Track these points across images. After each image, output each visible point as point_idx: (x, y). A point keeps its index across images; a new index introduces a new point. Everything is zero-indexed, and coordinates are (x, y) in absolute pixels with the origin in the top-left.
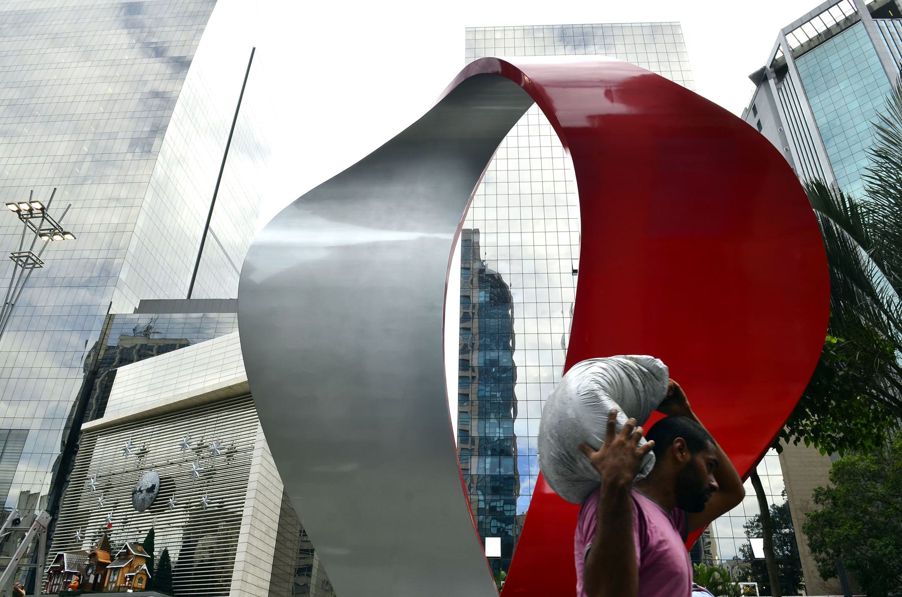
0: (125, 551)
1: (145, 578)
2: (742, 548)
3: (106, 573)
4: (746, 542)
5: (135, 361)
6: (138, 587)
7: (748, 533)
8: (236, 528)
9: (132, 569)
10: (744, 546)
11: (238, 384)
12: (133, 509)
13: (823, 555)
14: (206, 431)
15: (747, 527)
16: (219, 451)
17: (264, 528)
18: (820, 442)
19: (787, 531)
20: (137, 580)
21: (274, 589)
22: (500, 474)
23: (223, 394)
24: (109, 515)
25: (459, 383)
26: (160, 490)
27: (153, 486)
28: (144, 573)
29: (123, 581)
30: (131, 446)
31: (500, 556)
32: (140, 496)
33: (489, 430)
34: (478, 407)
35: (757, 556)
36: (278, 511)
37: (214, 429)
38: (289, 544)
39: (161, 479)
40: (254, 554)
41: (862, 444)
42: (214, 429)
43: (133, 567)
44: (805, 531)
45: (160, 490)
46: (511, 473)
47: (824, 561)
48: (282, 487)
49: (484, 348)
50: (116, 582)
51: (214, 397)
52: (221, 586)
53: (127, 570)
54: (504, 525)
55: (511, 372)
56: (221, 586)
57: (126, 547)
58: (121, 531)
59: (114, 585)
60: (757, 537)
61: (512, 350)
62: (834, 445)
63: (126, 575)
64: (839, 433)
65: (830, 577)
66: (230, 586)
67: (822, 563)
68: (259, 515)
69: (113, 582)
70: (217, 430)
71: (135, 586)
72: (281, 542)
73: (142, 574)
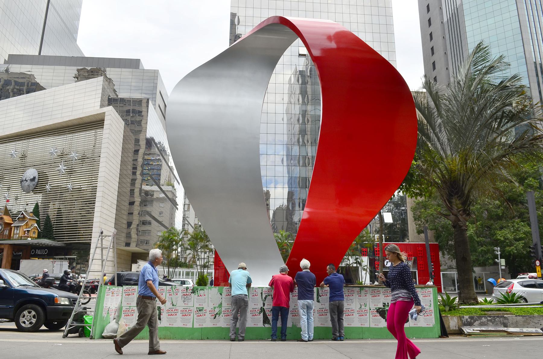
0: (22, 216)
1: (37, 231)
3: (11, 228)
5: (11, 97)
6: (33, 236)
9: (28, 227)
11: (86, 117)
12: (21, 191)
13: (420, 222)
16: (76, 158)
17: (109, 203)
19: (404, 208)
20: (32, 233)
23: (76, 122)
24: (6, 194)
26: (39, 180)
27: (34, 178)
28: (36, 228)
29: (23, 233)
30: (16, 153)
32: (27, 184)
38: (123, 212)
39: (39, 173)
40: (105, 218)
41: (425, 195)
43: (28, 225)
45: (39, 180)
47: (419, 225)
50: (19, 234)
53: (25, 227)
57: (22, 214)
58: (15, 204)
59: (17, 236)
60: (388, 212)
62: (413, 195)
63: (25, 230)
64: (416, 190)
69: (17, 234)
71: (31, 236)
73: (35, 229)
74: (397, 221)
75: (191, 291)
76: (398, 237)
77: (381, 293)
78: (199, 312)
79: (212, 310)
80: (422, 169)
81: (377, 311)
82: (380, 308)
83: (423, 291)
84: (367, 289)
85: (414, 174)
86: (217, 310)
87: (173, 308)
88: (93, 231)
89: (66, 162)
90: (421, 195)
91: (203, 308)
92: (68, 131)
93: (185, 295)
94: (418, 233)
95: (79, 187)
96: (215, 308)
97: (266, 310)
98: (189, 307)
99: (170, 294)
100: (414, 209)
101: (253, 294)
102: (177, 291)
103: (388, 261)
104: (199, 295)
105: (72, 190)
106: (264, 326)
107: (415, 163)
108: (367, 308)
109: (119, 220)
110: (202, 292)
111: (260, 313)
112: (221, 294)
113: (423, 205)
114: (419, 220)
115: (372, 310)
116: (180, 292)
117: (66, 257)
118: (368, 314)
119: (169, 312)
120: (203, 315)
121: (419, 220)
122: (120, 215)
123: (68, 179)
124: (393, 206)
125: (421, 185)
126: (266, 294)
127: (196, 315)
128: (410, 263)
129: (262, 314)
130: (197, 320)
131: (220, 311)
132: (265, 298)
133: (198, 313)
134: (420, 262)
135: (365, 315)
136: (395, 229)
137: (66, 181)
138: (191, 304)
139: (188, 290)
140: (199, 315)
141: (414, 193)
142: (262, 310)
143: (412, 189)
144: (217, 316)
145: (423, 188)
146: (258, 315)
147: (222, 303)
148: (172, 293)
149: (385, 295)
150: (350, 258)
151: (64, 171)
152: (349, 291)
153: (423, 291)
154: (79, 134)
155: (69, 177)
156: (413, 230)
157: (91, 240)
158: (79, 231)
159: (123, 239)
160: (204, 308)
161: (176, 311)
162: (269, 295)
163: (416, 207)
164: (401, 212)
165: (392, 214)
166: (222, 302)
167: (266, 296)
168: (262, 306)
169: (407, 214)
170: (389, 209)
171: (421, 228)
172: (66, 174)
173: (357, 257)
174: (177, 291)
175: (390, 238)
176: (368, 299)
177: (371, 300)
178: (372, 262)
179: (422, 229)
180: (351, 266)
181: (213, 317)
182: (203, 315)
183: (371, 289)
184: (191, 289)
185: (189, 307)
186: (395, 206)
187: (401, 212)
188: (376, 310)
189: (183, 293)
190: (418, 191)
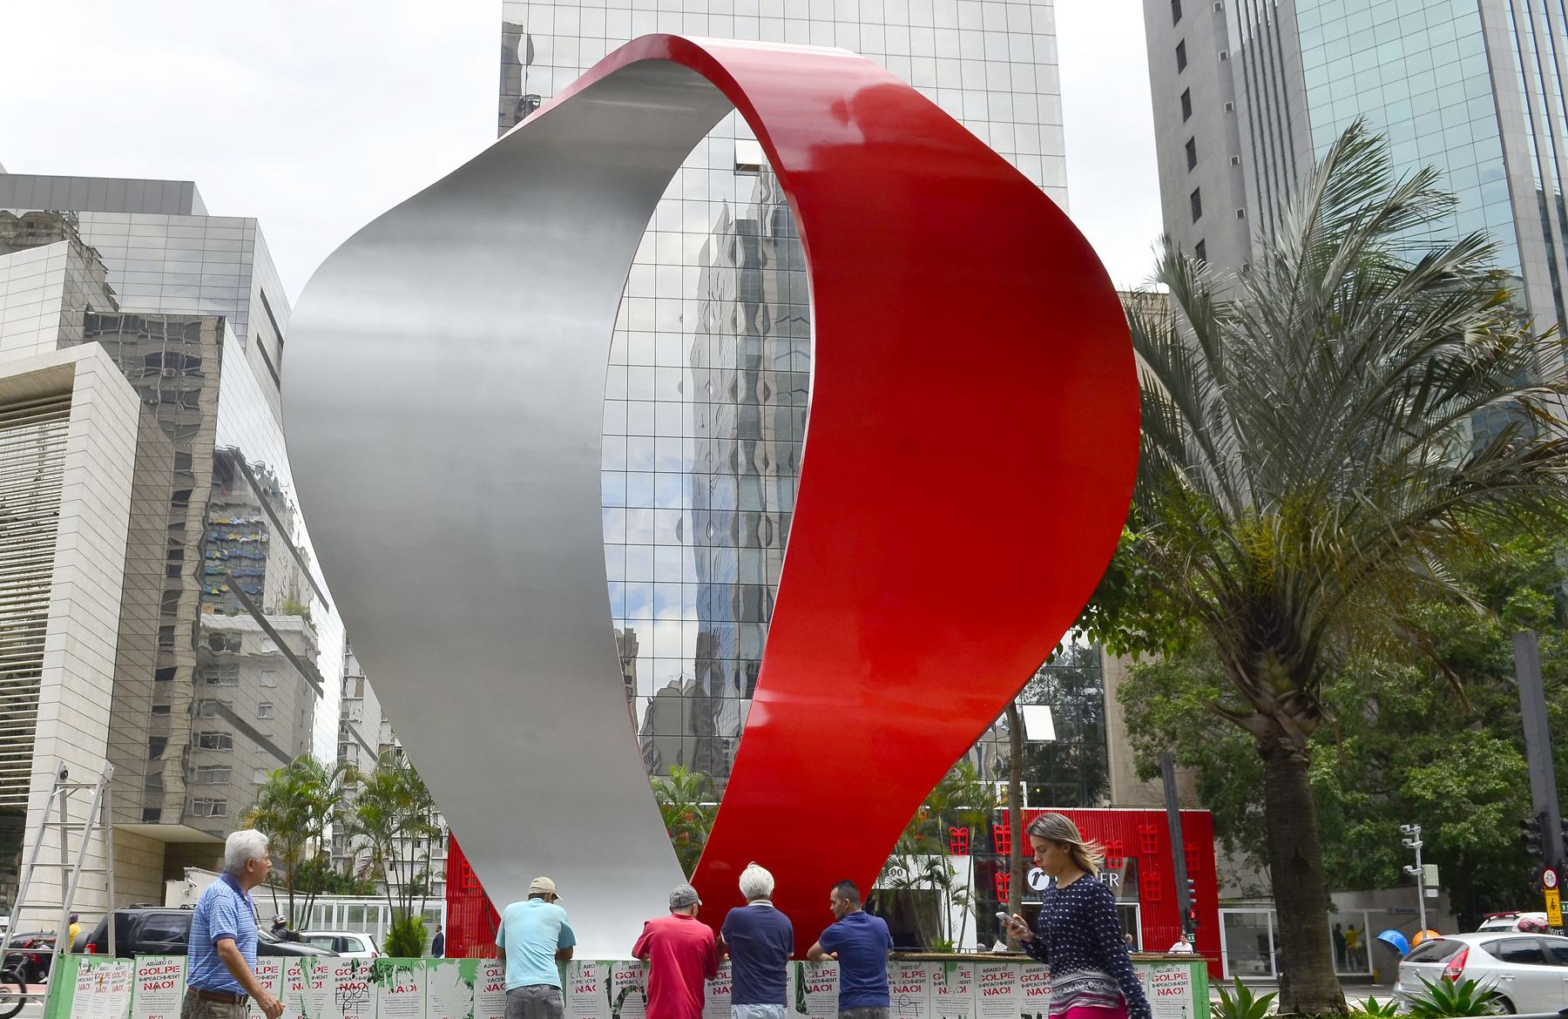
8: (36, 649)
17: (88, 675)
19: (1092, 691)
35: (1032, 734)
36: (113, 640)
38: (135, 703)
60: (1038, 703)
62: (1126, 646)
67: (1144, 750)
74: (1071, 734)
75: (367, 974)
76: (1073, 790)
83: (1159, 975)
84: (967, 967)
85: (1128, 574)
88: (33, 770)
90: (1151, 646)
93: (346, 988)
94: (1141, 775)
99: (297, 983)
100: (1127, 694)
101: (579, 985)
102: (319, 973)
103: (1040, 870)
104: (396, 989)
107: (1132, 537)
110: (404, 978)
112: (470, 985)
114: (1146, 732)
121: (1144, 733)
122: (125, 716)
124: (1056, 682)
126: (625, 986)
132: (621, 998)
134: (1147, 876)
141: (1127, 637)
143: (1120, 624)
145: (1159, 622)
148: (303, 982)
152: (905, 975)
153: (1159, 975)
157: (26, 799)
162: (634, 989)
163: (1134, 688)
164: (1085, 705)
165: (1053, 712)
166: (472, 1011)
167: (624, 990)
170: (1042, 694)
174: (319, 973)
175: (1045, 791)
176: (971, 1005)
177: (979, 1004)
178: (984, 876)
180: (914, 887)
186: (1063, 685)
189: (340, 982)
190: (1141, 633)
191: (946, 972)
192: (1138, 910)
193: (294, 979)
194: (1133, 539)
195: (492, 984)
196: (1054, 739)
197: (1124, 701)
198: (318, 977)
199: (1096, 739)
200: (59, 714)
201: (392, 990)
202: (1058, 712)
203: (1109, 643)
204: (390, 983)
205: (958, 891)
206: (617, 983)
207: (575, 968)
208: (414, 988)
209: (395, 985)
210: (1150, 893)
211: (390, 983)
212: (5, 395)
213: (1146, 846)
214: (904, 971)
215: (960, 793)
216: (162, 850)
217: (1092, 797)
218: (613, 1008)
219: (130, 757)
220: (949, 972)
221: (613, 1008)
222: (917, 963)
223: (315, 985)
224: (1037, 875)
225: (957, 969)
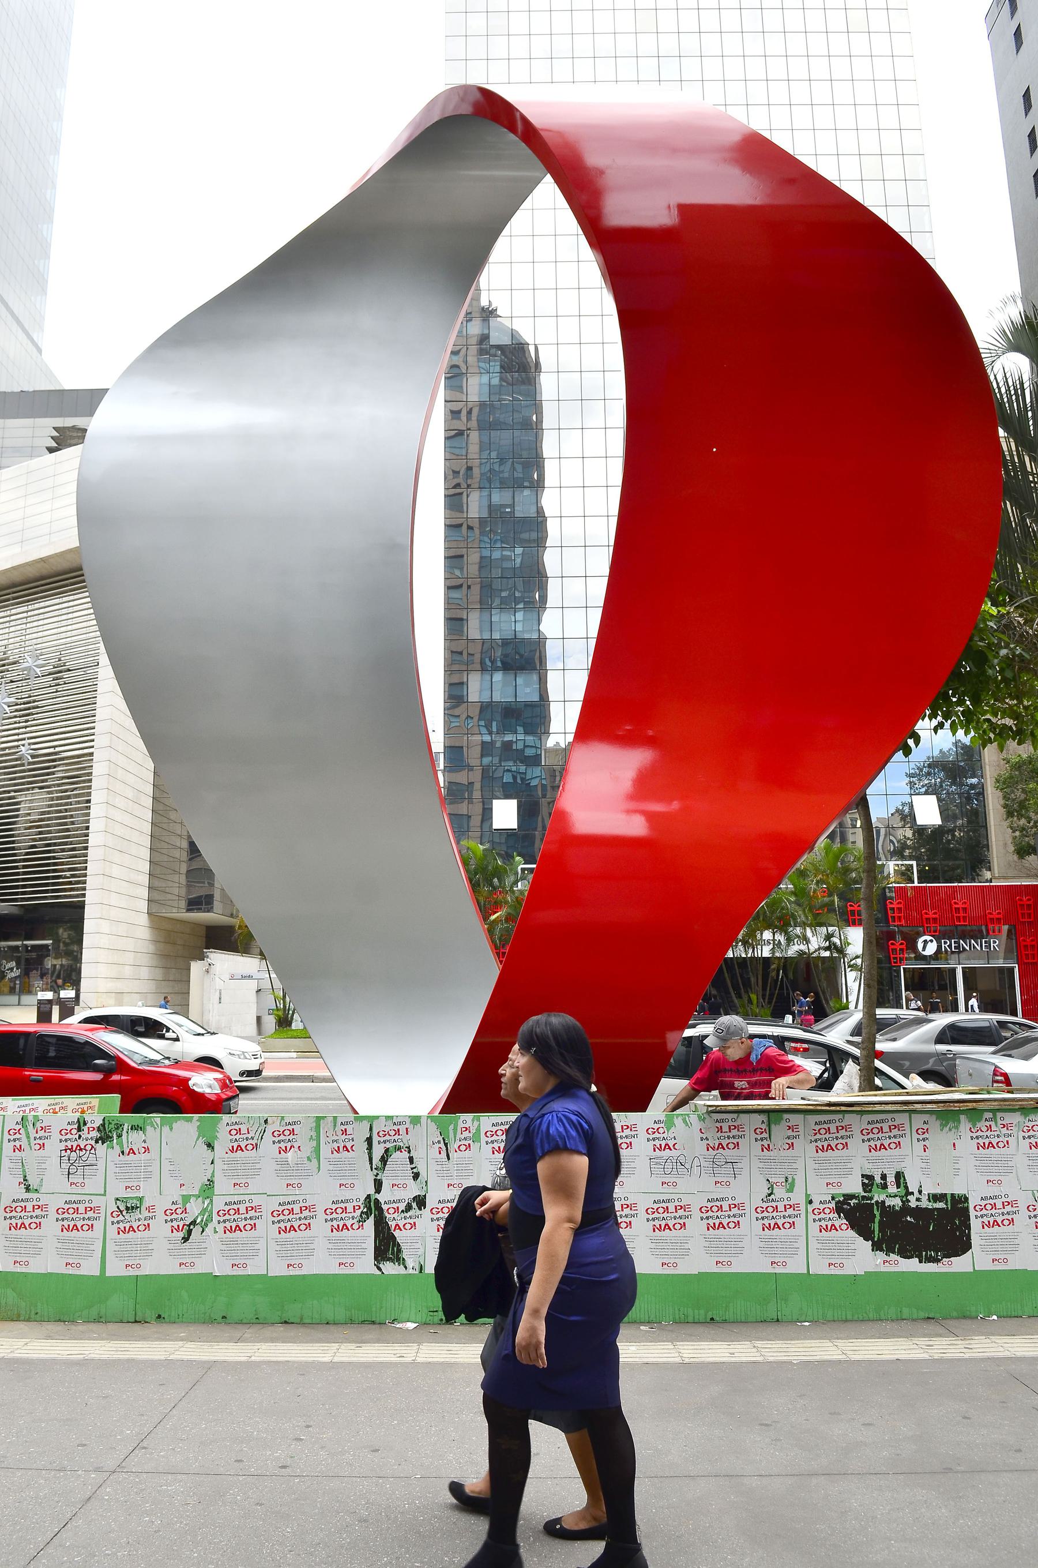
2: (901, 808)
4: (907, 799)
7: (911, 784)
10: (903, 805)
13: (1023, 821)
14: (12, 623)
15: (911, 776)
16: (38, 670)
18: (973, 727)
19: (974, 781)
21: (157, 883)
22: (516, 701)
23: (32, 573)
25: (446, 537)
31: (516, 827)
33: (500, 617)
34: (479, 585)
37: (24, 621)
40: (119, 834)
42: (24, 621)
44: (997, 787)
46: (536, 698)
48: (151, 765)
49: (488, 482)
51: (17, 577)
52: (70, 883)
54: (522, 769)
55: (538, 523)
56: (70, 883)
60: (926, 793)
61: (539, 485)
62: (992, 736)
65: (1029, 854)
66: (87, 863)
67: (1021, 832)
68: (120, 774)
70: (30, 616)
72: (160, 812)
74: (955, 818)
75: (95, 1134)
76: (958, 867)
77: (856, 1132)
78: (127, 1216)
79: (174, 1207)
80: (1022, 636)
81: (839, 1209)
82: (852, 1197)
83: (1030, 1124)
84: (795, 1119)
85: (990, 656)
86: (194, 1209)
87: (27, 1200)
88: (88, 872)
89: (14, 685)
90: (1020, 735)
91: (141, 1199)
92: (14, 598)
93: (71, 1150)
94: (1018, 853)
95: (52, 750)
96: (186, 1199)
97: (385, 1207)
98: (87, 1198)
99: (17, 1144)
100: (1004, 783)
101: (336, 1145)
102: (41, 1133)
103: (928, 938)
104: (126, 1151)
105: (31, 760)
106: (379, 1269)
107: (994, 611)
108: (798, 1197)
109: (163, 839)
110: (135, 1139)
111: (362, 1221)
112: (210, 1146)
113: (1032, 771)
114: (1022, 816)
115: (816, 1204)
116: (56, 1136)
117: (25, 942)
118: (800, 1222)
119: (14, 1214)
120: (142, 1228)
121: (1020, 816)
122: (165, 826)
123: (21, 730)
124: (942, 774)
125: (1019, 698)
126: (388, 1145)
127: (116, 1226)
128: (995, 942)
129: (370, 1223)
130: (117, 1248)
131: (204, 1210)
132: (384, 1160)
133: (121, 1218)
134: (1024, 940)
135: (787, 1225)
136: (949, 842)
137: (16, 737)
138: (94, 1185)
139: (85, 1128)
140: (127, 1226)
141: (993, 727)
142: (370, 1209)
143: (985, 713)
144: (196, 1231)
145: (1026, 708)
146: (355, 1226)
147: (215, 1179)
148: (24, 1143)
149: (872, 1144)
150: (809, 933)
151: (7, 709)
152: (720, 1129)
153: (1030, 1124)
154: (42, 604)
155: (24, 724)
156: (1005, 845)
157: (84, 895)
158: (55, 871)
159: (176, 891)
160: (146, 1199)
161: (38, 1212)
162: (399, 1149)
163: (1011, 777)
164: (968, 793)
165: (939, 800)
166: (213, 1175)
167: (387, 1150)
168: (371, 1190)
169: (984, 797)
170: (929, 786)
171: (1027, 839)
172: (15, 717)
173: (830, 929)
174: (41, 1133)
175: (933, 869)
176: (800, 1165)
177: (811, 1165)
178: (878, 942)
179: (1032, 842)
180: (815, 955)
181: (181, 1234)
182: (142, 1228)
183: (813, 1119)
184: (96, 1125)
185: (87, 1198)
186: (947, 777)
187: (968, 793)
188: (833, 1205)
189: (64, 1144)
190: (1009, 722)
191: (769, 1125)
192: (1016, 970)
193: (14, 1140)
194: (995, 614)
195: (235, 1145)
196: (940, 823)
197: (1001, 789)
198: (40, 1138)
199: (978, 823)
200: (106, 825)
201: (123, 1153)
202: (944, 800)
203: (972, 733)
204: (121, 1144)
205: (851, 961)
206: (379, 1142)
207: (330, 1125)
208: (147, 1150)
209: (125, 1146)
210: (1027, 955)
211: (121, 1144)
212: (54, 568)
213: (1023, 914)
214: (718, 1125)
215: (854, 875)
216: (203, 932)
217: (976, 872)
218: (375, 1172)
219: (172, 859)
220: (773, 1126)
221: (375, 1172)
222: (735, 1116)
223: (38, 1147)
224: (926, 942)
225: (783, 1123)
